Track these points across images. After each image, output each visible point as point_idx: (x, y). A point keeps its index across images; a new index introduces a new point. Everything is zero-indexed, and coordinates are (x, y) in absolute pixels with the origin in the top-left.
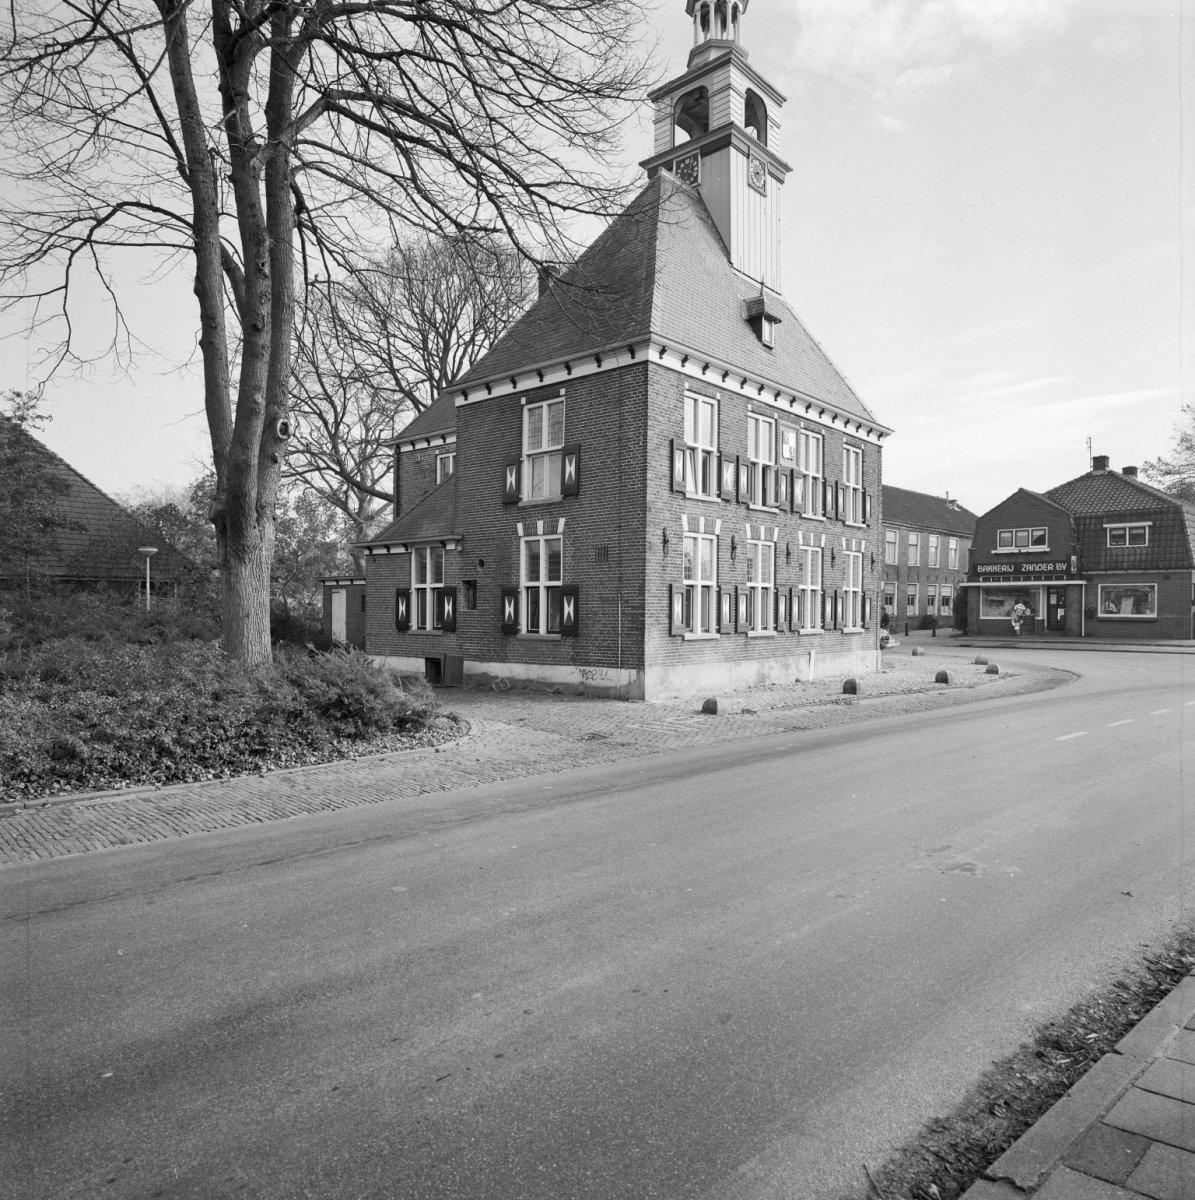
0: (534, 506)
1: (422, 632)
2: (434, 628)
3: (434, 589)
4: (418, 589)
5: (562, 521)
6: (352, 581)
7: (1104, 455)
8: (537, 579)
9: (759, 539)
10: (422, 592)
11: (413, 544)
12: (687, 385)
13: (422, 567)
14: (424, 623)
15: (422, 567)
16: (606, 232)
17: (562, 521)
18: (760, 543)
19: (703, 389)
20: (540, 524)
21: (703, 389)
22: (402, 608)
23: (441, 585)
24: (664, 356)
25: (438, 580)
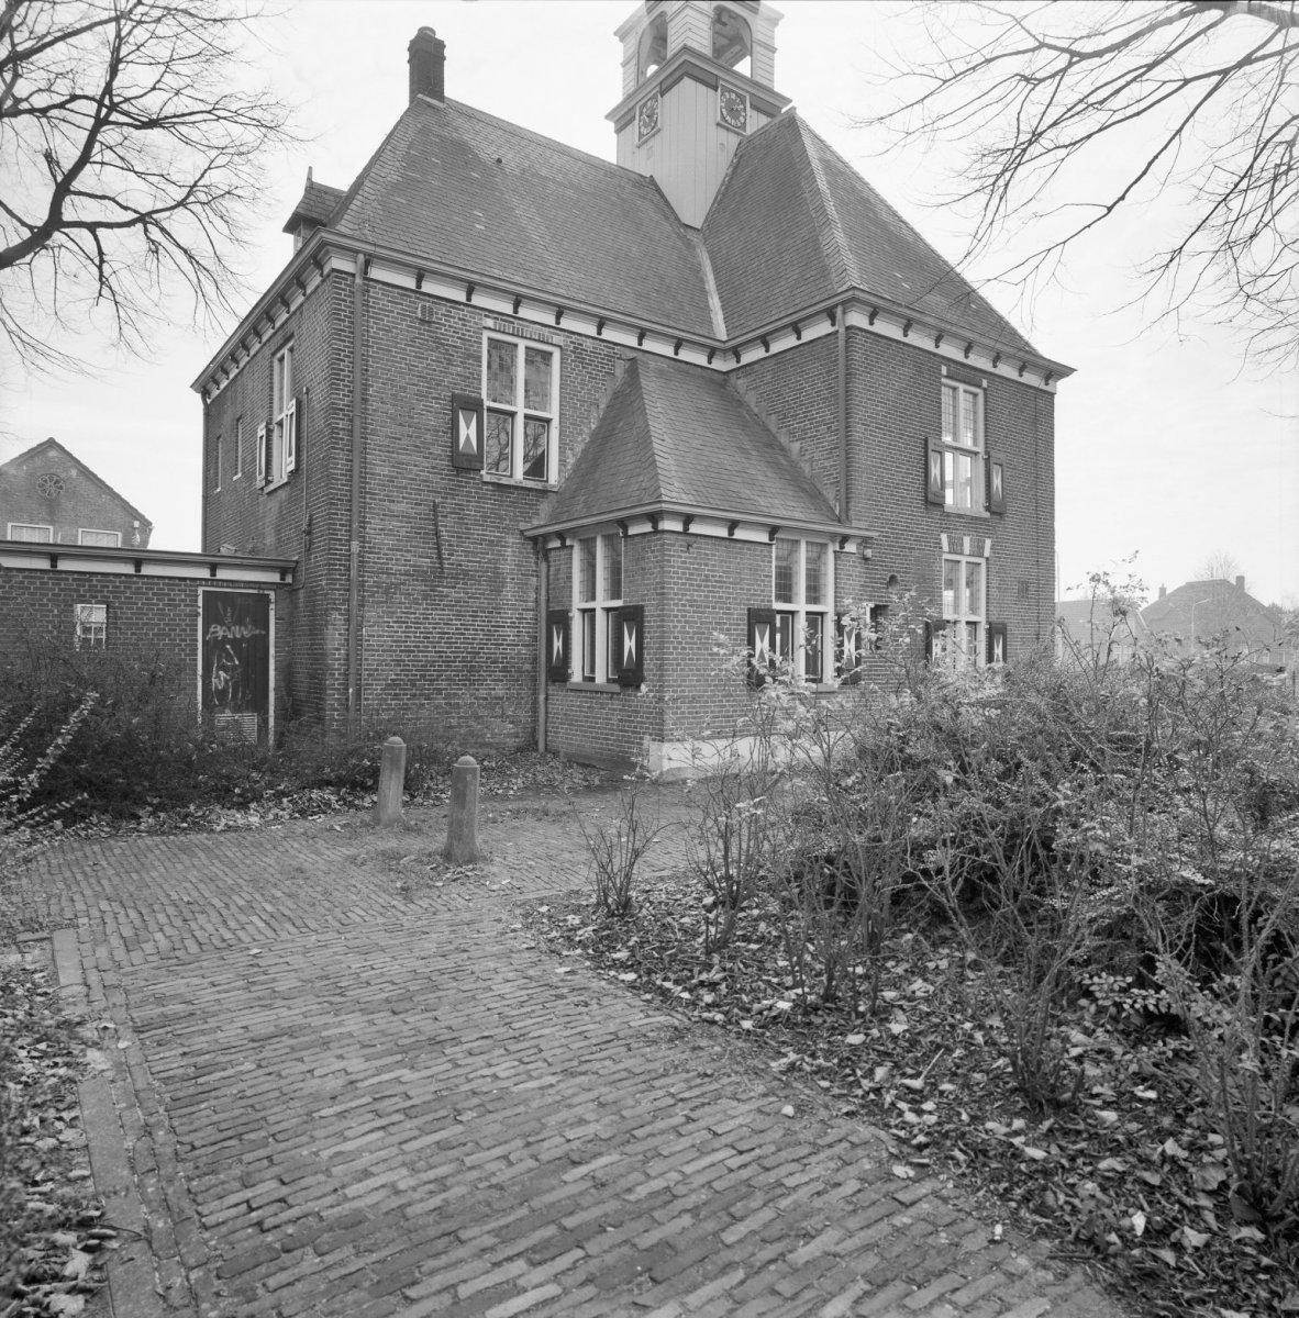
0: (960, 516)
1: (589, 685)
2: (608, 680)
3: (608, 610)
4: (584, 611)
5: (988, 543)
6: (54, 559)
7: (413, 34)
8: (593, 598)
9: (961, 554)
10: (589, 614)
11: (573, 532)
12: (944, 370)
13: (590, 567)
14: (593, 670)
15: (590, 567)
16: (945, 263)
17: (988, 543)
18: (964, 559)
19: (969, 375)
20: (967, 540)
21: (969, 375)
22: (558, 644)
23: (618, 603)
24: (999, 365)
25: (616, 594)
